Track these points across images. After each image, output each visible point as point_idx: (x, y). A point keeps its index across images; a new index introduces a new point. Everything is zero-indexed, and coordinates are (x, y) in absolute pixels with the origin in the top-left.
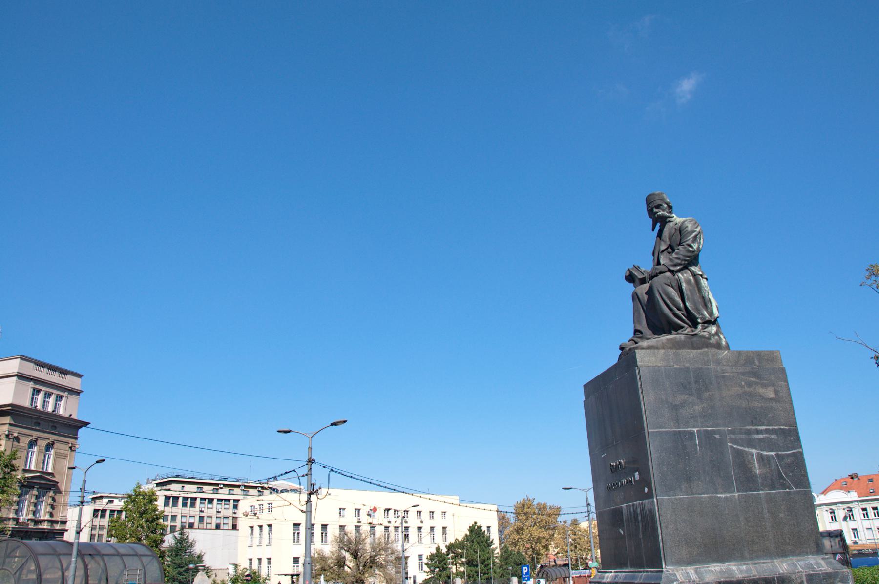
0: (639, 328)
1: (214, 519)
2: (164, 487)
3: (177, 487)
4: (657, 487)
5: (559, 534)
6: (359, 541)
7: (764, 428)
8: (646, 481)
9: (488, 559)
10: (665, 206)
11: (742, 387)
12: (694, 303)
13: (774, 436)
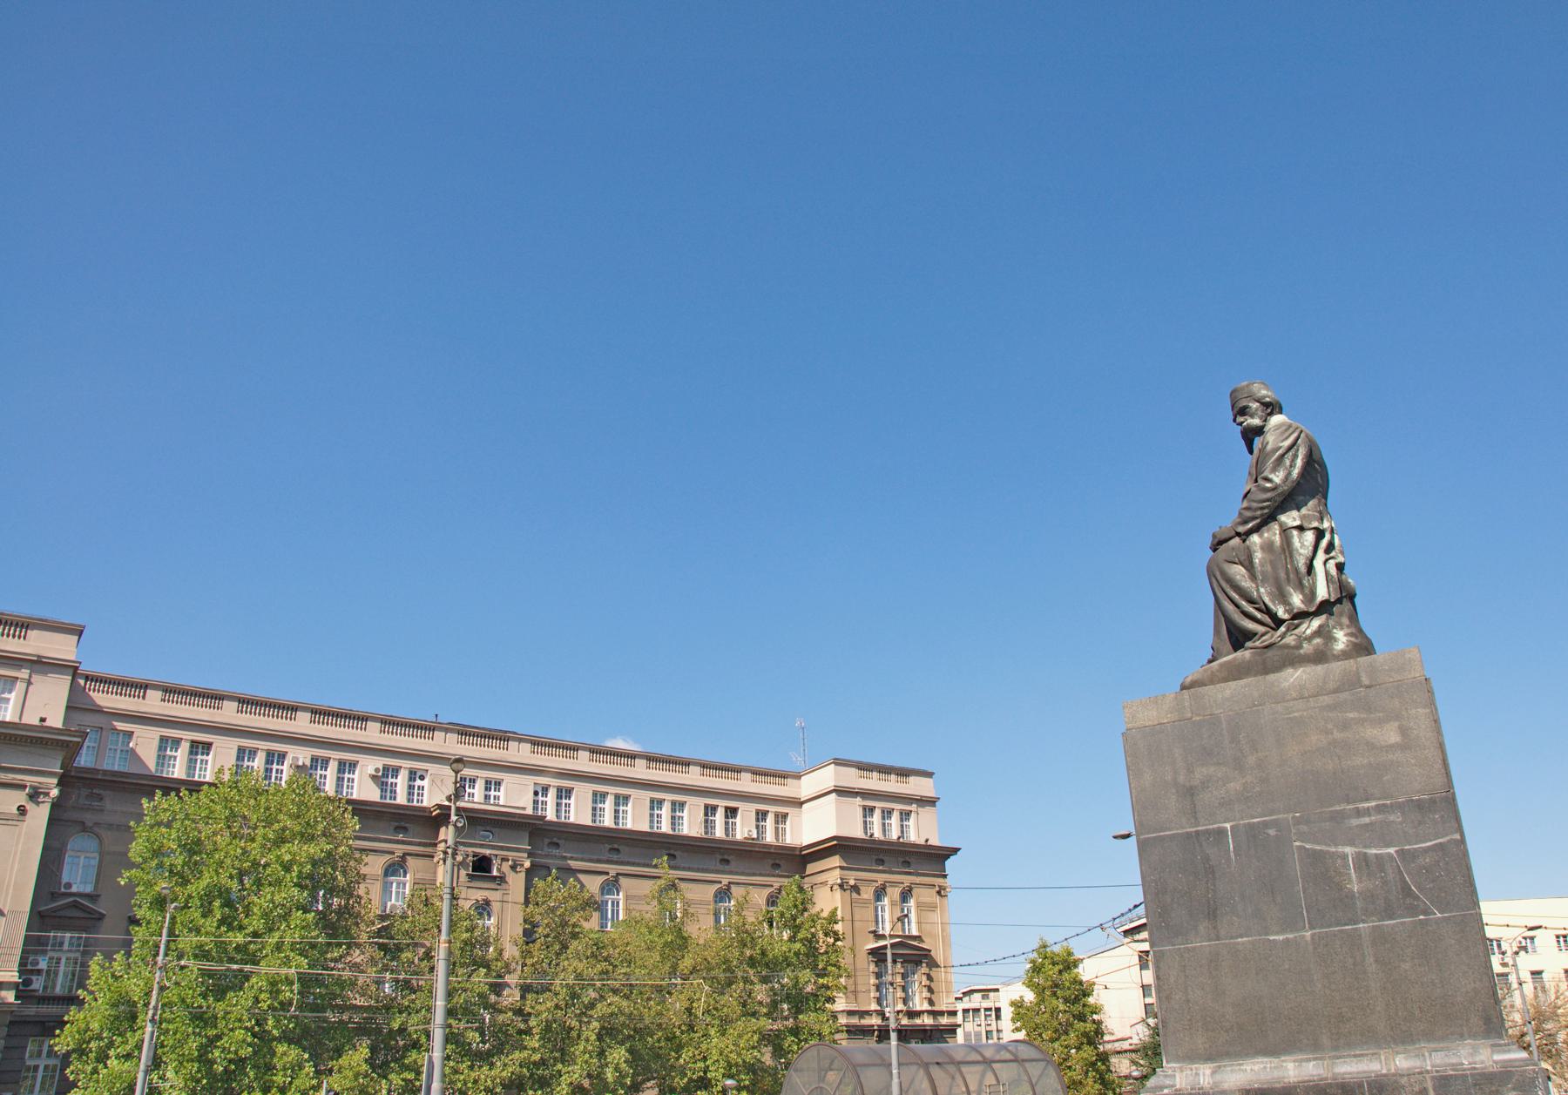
2: (1137, 937)
10: (1255, 405)
11: (1328, 732)
13: (1396, 817)
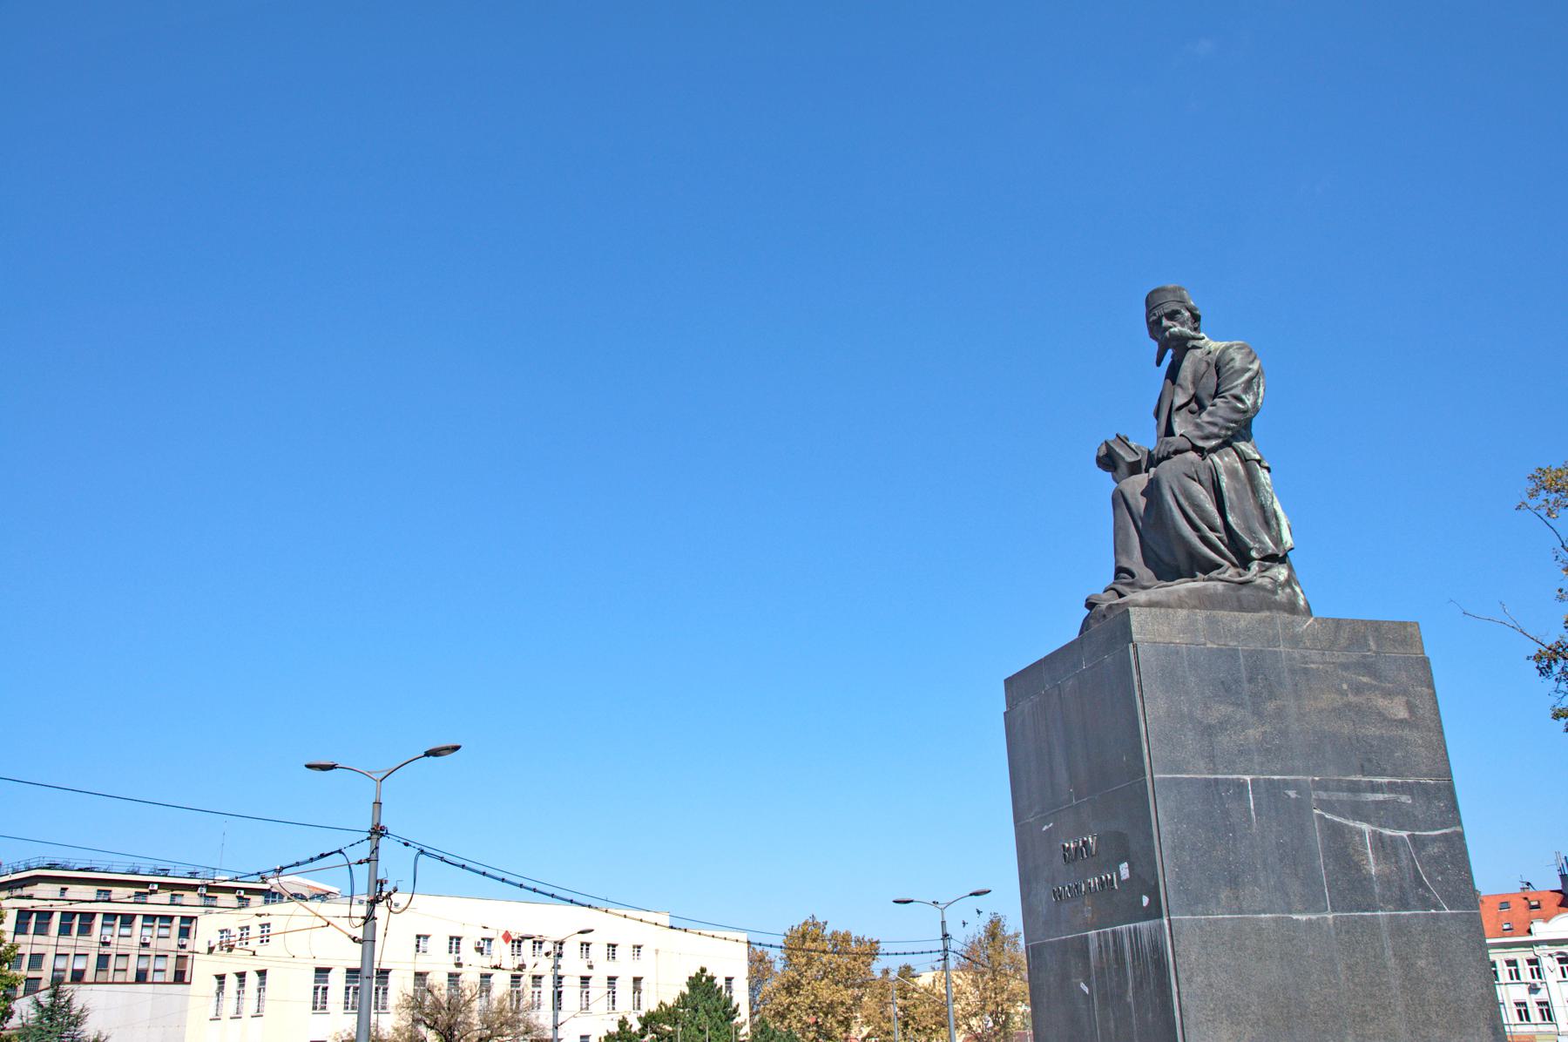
0: (1125, 563)
1: (133, 959)
2: (18, 892)
3: (51, 890)
4: (1171, 894)
5: (873, 996)
7: (1386, 780)
10: (1187, 314)
11: (1343, 693)
12: (1244, 517)
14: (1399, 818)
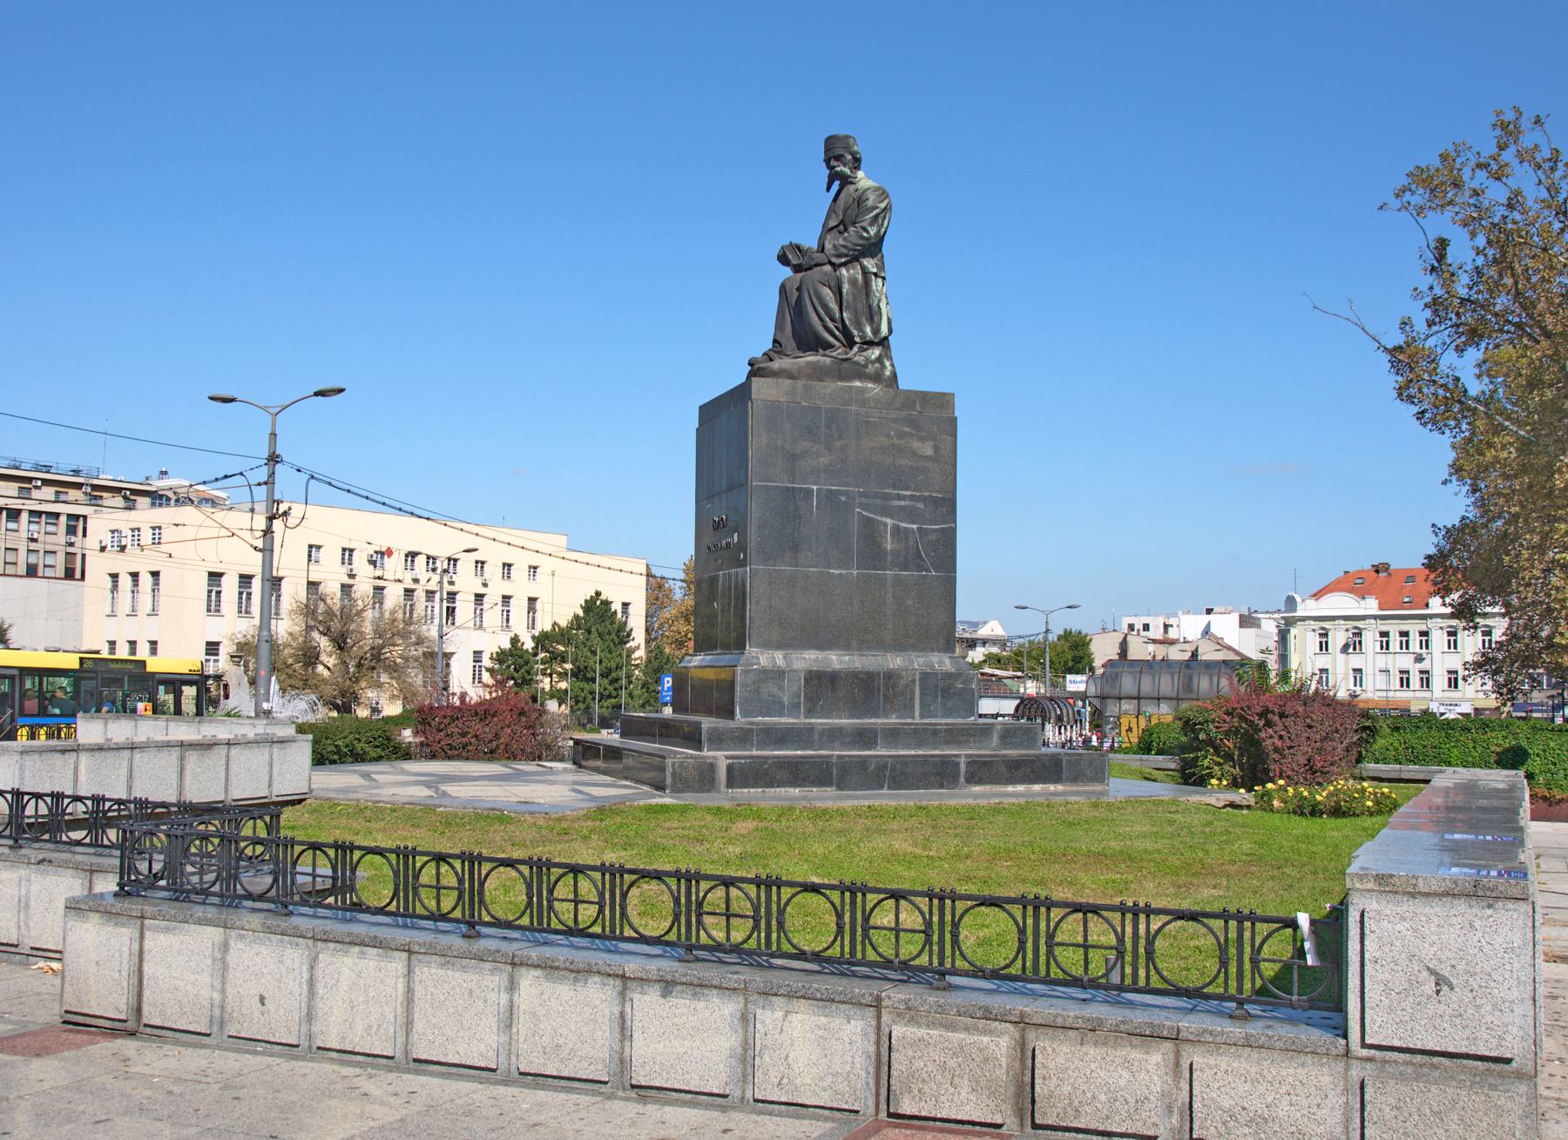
6: (349, 613)
8: (742, 546)
9: (619, 667)
11: (888, 436)
13: (920, 505)
14: (911, 515)
